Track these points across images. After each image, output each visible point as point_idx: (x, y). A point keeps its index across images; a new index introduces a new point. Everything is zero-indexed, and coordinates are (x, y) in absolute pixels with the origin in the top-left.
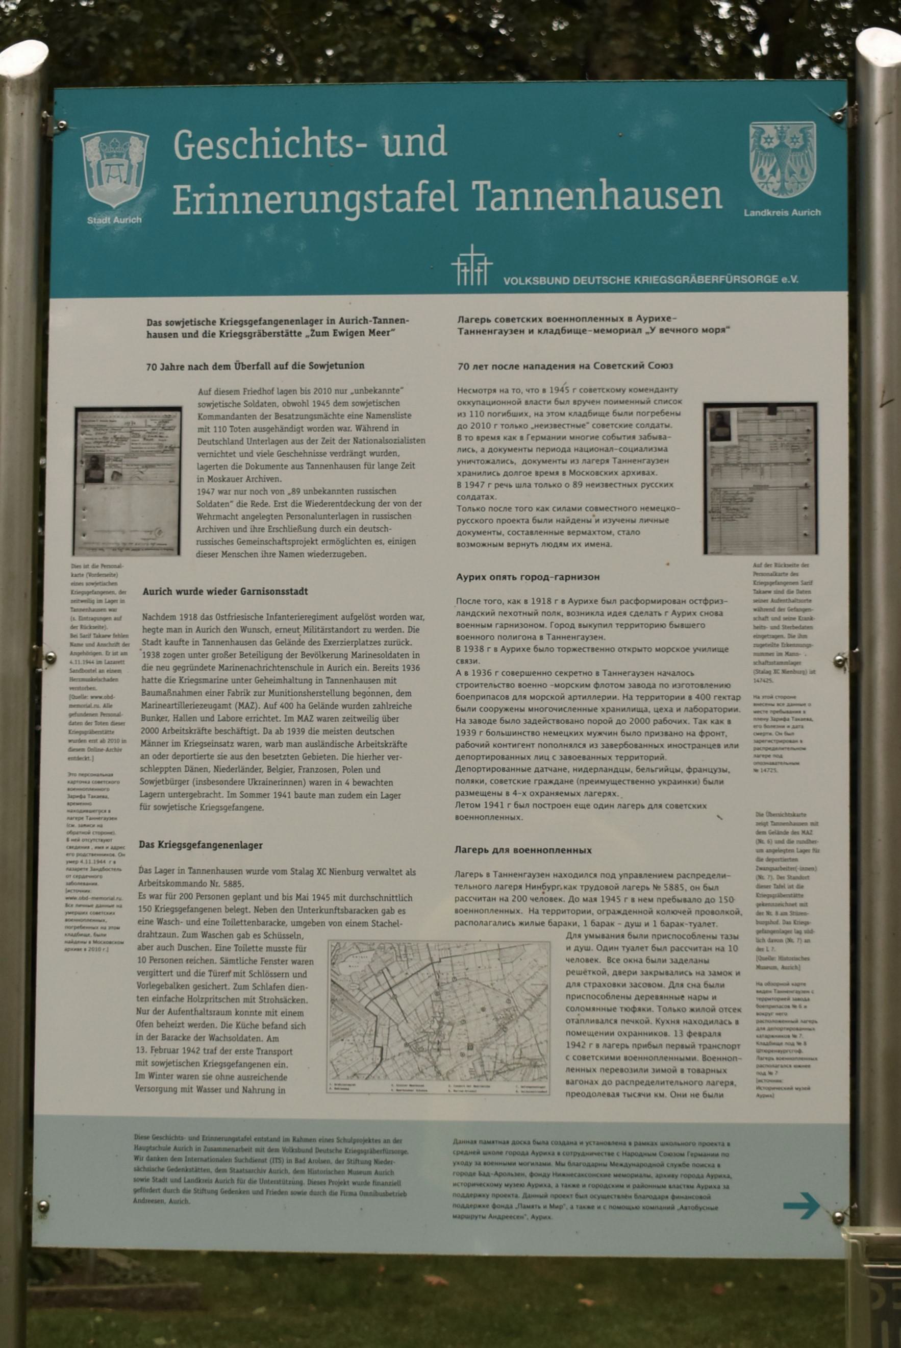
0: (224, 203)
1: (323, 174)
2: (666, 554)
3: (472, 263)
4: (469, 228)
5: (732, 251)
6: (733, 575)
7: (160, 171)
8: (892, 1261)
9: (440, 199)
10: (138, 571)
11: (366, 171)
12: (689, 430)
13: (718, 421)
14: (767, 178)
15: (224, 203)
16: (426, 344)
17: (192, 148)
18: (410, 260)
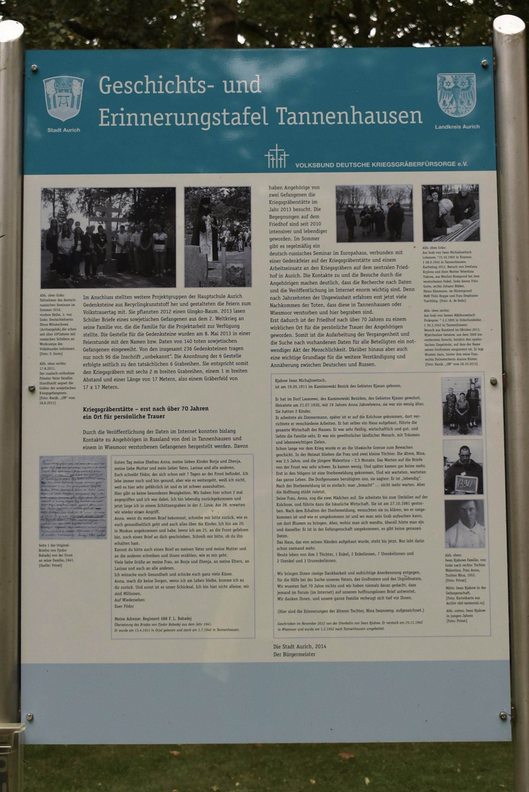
0: (130, 119)
7: (92, 100)
14: (448, 106)
15: (130, 119)
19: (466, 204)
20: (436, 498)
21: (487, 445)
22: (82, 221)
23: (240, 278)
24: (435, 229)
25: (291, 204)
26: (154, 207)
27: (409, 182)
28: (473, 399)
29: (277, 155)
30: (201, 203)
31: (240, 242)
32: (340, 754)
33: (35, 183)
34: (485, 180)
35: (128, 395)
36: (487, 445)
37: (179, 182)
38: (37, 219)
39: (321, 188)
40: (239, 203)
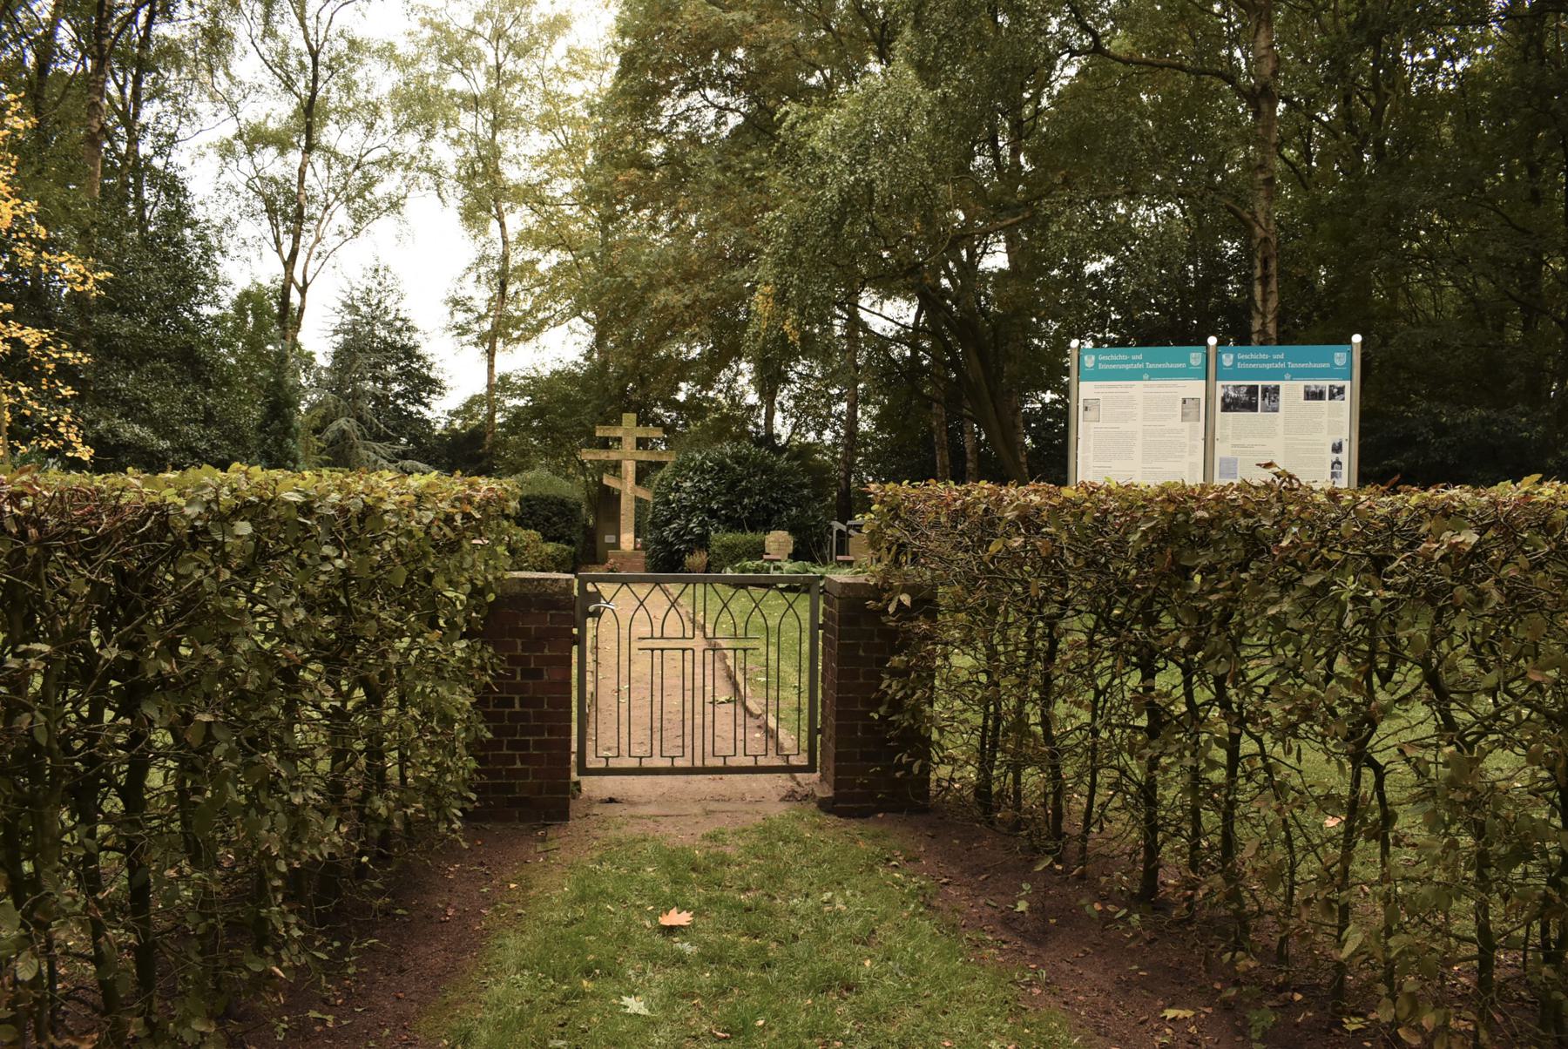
0: (1106, 367)
1: (1262, 361)
2: (1176, 421)
3: (1146, 376)
4: (1286, 370)
5: (1187, 374)
6: (1187, 424)
7: (1236, 360)
8: (637, 569)
9: (1283, 365)
10: (1093, 425)
11: (1129, 361)
12: (1180, 402)
13: (1184, 401)
14: (1337, 362)
15: (1106, 367)
16: (1138, 388)
17: (1240, 357)
18: (1136, 375)
19: (1341, 390)
20: (1329, 471)
21: (1343, 457)
22: (1232, 394)
23: (1276, 410)
24: (1332, 397)
25: (1292, 391)
26: (1252, 390)
27: (1325, 384)
28: (1340, 444)
29: (1287, 376)
30: (1265, 389)
31: (1276, 400)
32: (63, 23)
33: (1220, 383)
34: (1347, 384)
35: (1243, 441)
36: (1343, 457)
37: (1260, 383)
38: (1220, 393)
39: (1300, 386)
40: (1276, 390)
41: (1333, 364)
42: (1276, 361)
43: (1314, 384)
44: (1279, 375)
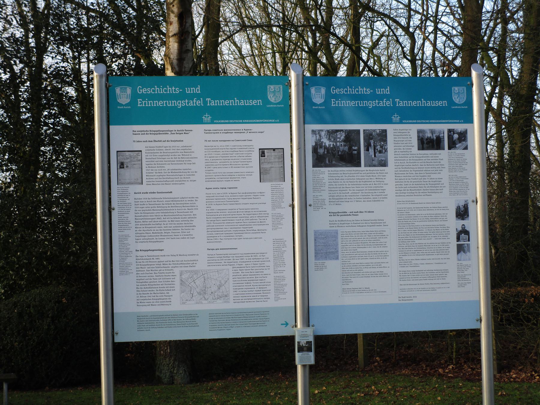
0: (150, 103)
2: (251, 182)
3: (396, 118)
4: (395, 109)
6: (266, 187)
7: (135, 96)
9: (388, 103)
10: (133, 189)
11: (182, 96)
13: (262, 153)
15: (150, 103)
18: (192, 117)
22: (327, 142)
23: (384, 164)
26: (351, 137)
27: (442, 128)
29: (207, 117)
30: (369, 135)
33: (310, 127)
37: (361, 127)
39: (412, 130)
40: (383, 135)
41: (451, 103)
42: (191, 97)
43: (430, 128)
44: (384, 116)
